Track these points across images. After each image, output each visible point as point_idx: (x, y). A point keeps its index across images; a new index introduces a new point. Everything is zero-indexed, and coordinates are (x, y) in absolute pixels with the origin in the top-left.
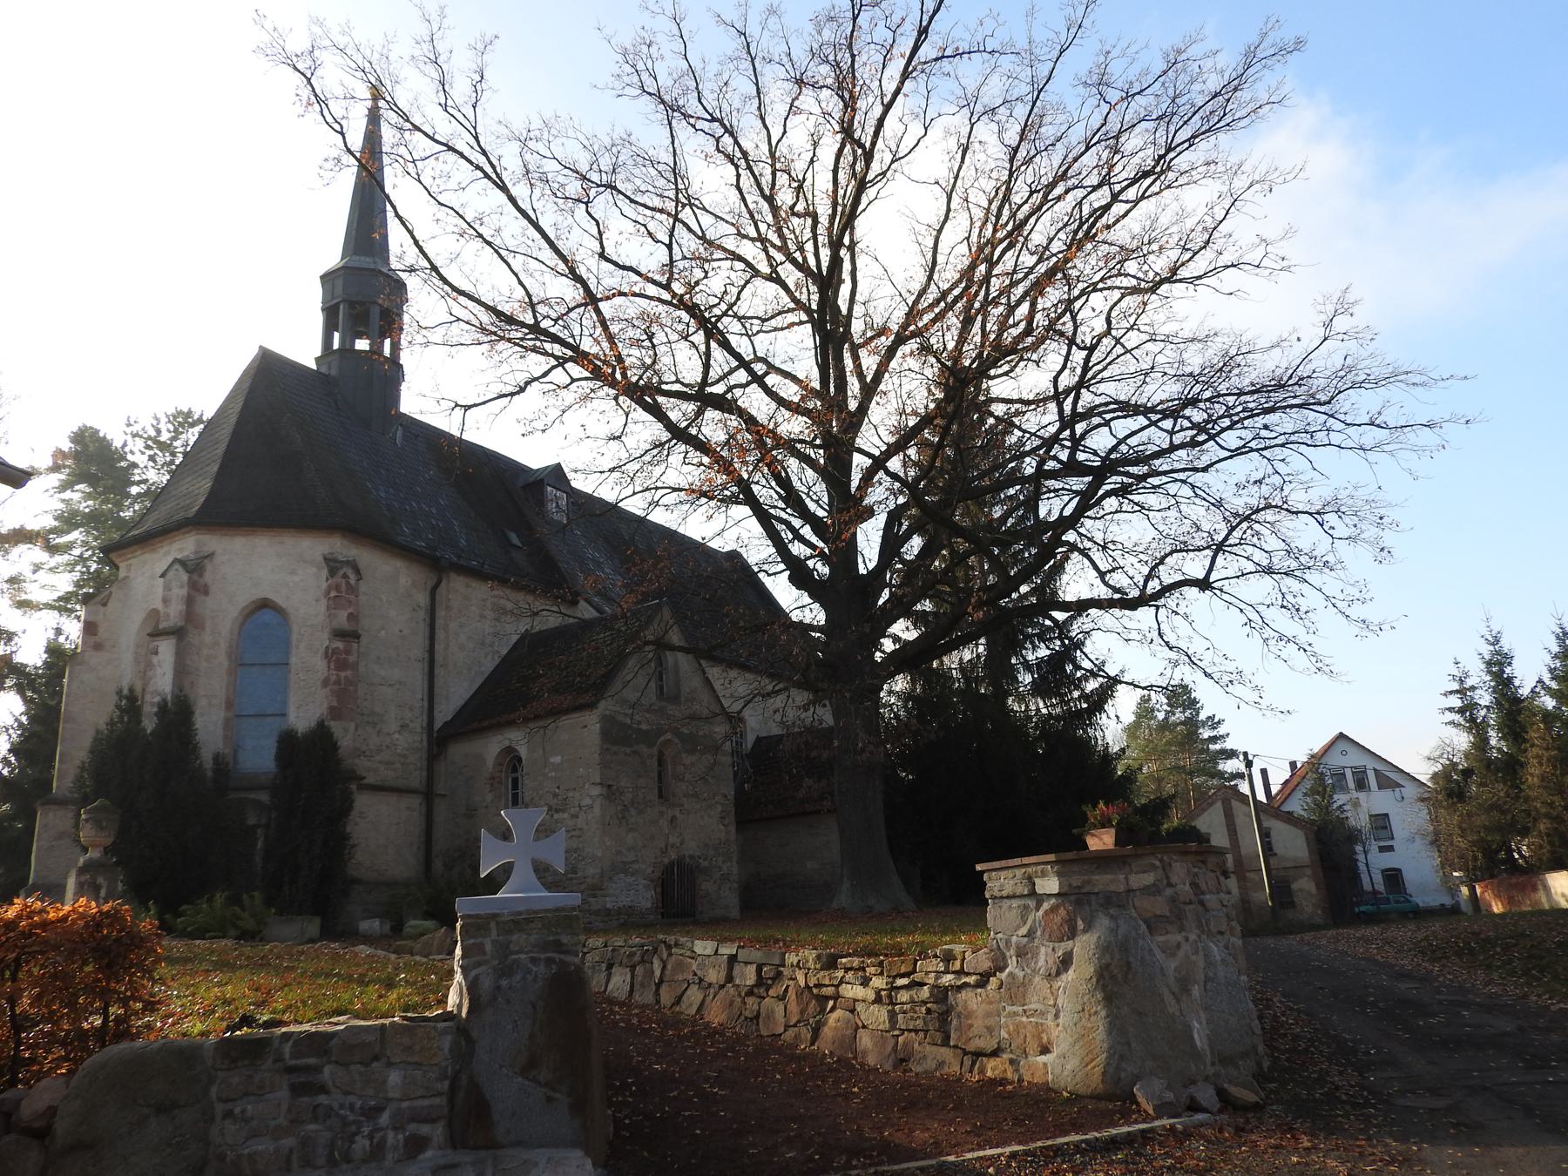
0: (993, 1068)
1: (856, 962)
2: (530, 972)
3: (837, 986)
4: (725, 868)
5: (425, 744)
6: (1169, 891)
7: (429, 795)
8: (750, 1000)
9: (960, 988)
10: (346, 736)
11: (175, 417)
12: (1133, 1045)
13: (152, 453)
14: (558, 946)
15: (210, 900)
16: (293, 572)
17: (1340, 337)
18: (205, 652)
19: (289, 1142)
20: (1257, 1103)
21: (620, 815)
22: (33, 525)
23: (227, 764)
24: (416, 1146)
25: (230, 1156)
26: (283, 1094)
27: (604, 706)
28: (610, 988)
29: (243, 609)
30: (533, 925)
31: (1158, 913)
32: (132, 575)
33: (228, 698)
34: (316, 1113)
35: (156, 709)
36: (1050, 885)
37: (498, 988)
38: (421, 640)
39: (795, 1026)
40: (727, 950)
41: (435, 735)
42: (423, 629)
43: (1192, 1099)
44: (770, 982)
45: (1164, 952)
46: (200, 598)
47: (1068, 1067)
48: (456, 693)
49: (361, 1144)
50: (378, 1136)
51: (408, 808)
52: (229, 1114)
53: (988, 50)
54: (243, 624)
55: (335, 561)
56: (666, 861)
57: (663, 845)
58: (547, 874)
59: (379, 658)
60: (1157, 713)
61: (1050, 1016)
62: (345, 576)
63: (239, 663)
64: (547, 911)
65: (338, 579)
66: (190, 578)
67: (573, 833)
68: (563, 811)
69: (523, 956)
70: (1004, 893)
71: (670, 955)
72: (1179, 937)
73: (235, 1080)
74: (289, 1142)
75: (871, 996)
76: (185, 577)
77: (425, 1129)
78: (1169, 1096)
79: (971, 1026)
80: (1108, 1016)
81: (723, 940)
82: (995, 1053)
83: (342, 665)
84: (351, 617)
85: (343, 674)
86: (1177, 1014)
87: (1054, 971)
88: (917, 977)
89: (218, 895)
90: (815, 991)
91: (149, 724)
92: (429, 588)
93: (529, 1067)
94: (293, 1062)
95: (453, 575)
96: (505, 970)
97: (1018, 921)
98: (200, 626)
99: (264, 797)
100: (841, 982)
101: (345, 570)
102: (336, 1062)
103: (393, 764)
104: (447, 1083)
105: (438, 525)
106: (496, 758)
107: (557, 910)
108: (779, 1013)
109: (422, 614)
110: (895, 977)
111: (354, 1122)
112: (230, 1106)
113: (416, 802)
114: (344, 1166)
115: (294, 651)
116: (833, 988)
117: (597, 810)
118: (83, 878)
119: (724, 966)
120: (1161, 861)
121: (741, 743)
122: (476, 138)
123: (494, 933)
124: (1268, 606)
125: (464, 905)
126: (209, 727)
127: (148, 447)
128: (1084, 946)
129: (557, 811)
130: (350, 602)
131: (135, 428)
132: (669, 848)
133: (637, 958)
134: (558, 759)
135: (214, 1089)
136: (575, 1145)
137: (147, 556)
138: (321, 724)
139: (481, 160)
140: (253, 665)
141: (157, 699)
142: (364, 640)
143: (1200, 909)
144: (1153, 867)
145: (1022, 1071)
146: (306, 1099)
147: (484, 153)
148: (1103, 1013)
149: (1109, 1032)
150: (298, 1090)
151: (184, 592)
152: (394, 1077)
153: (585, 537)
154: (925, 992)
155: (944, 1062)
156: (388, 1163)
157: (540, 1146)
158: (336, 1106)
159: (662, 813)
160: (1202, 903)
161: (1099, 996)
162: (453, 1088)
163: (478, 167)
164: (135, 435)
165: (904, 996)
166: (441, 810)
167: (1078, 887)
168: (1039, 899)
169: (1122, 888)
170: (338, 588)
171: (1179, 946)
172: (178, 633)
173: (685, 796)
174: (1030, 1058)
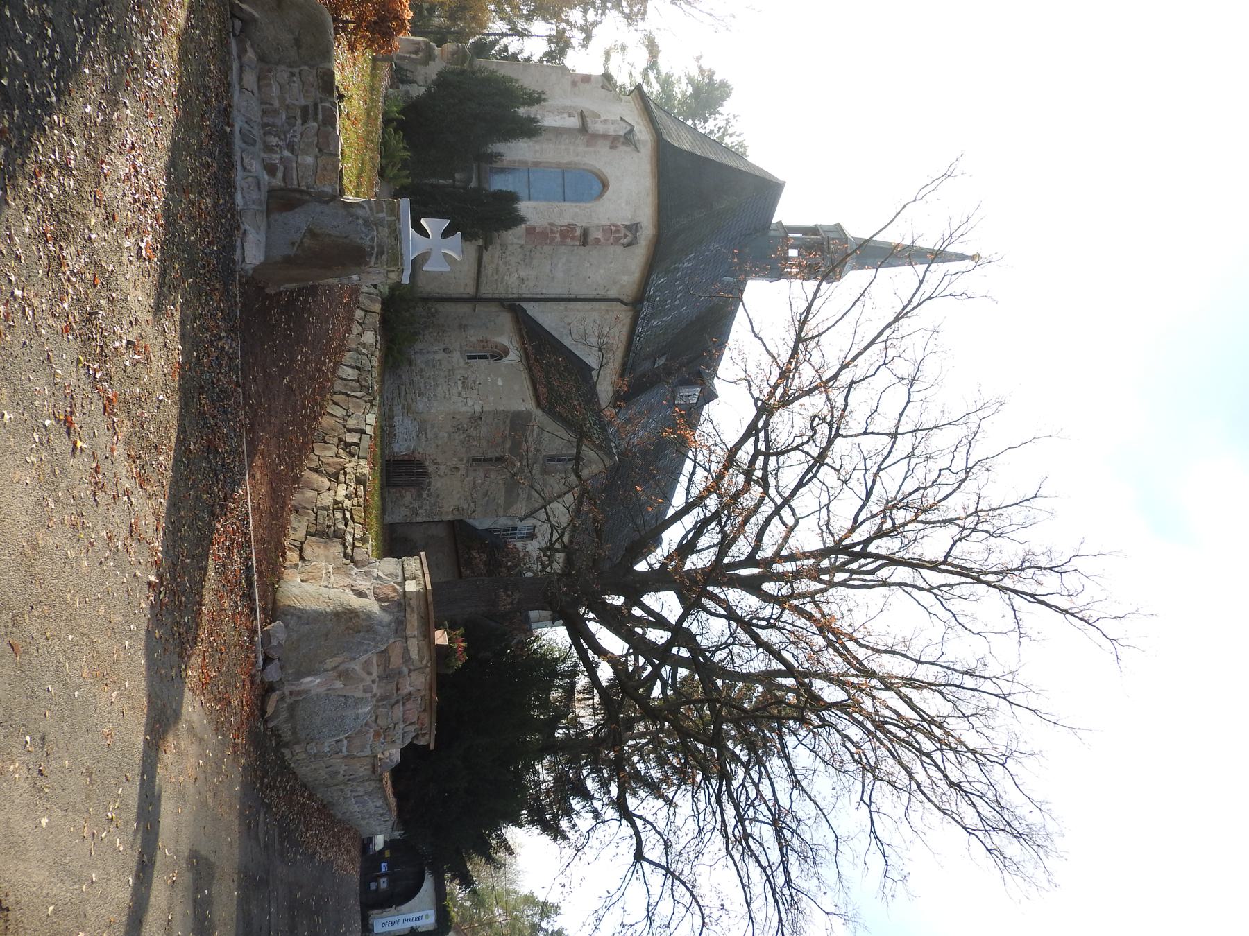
0: (293, 556)
1: (361, 493)
2: (367, 236)
3: (345, 483)
4: (421, 511)
5: (510, 296)
6: (405, 670)
7: (475, 299)
8: (336, 441)
9: (344, 545)
10: (514, 236)
11: (741, 146)
12: (307, 626)
13: (716, 131)
14: (381, 253)
15: (405, 148)
16: (627, 203)
17: (829, 926)
18: (572, 148)
19: (276, 104)
20: (266, 712)
21: (460, 427)
22: (661, 60)
23: (496, 162)
24: (271, 170)
25: (270, 75)
26: (303, 102)
27: (539, 416)
28: (345, 367)
29: (601, 171)
30: (393, 239)
31: (392, 660)
32: (622, 104)
33: (540, 163)
34: (291, 119)
35: (532, 116)
36: (411, 587)
37: (357, 218)
38: (584, 292)
39: (319, 460)
40: (369, 430)
41: (517, 303)
42: (591, 293)
43: (272, 660)
44: (348, 450)
45: (366, 662)
46: (608, 143)
47: (294, 589)
48: (547, 317)
49: (273, 140)
50: (278, 149)
51: (466, 285)
52: (293, 75)
53: (1021, 639)
54: (591, 172)
55: (637, 231)
56: (427, 463)
57: (438, 461)
58: (419, 377)
59: (570, 262)
60: (545, 920)
61: (326, 584)
62: (626, 236)
63: (564, 170)
64: (401, 249)
65: (623, 231)
66: (621, 136)
67: (447, 393)
68: (463, 387)
69: (375, 233)
70: (405, 566)
71: (366, 402)
72: (375, 675)
73: (311, 79)
74: (276, 104)
75: (338, 499)
76: (622, 133)
77: (280, 175)
78: (274, 643)
79: (319, 548)
80: (326, 612)
81: (375, 428)
82: (302, 558)
83: (564, 235)
84: (598, 240)
85: (558, 235)
86: (325, 667)
87: (353, 588)
88: (351, 523)
89: (409, 154)
90: (342, 472)
91: (522, 111)
92: (620, 297)
93: (312, 233)
94: (320, 107)
95: (630, 314)
96: (367, 223)
97: (388, 572)
98: (588, 144)
99: (473, 184)
100: (348, 485)
101: (630, 235)
102: (319, 129)
103: (497, 274)
104: (305, 188)
105: (666, 305)
106: (500, 343)
107: (401, 255)
108: (327, 453)
109: (602, 292)
110: (351, 512)
111: (286, 137)
112: (297, 75)
113: (471, 290)
114: (262, 132)
115: (573, 204)
116: (344, 480)
117: (464, 409)
118: (422, 44)
119: (359, 427)
120: (426, 666)
121: (515, 538)
122: (929, 298)
123: (389, 219)
124: (623, 908)
125: (405, 203)
126: (518, 151)
127: (720, 128)
128: (370, 605)
129: (463, 383)
130: (608, 240)
131: (732, 121)
132: (436, 466)
133: (364, 383)
134: (500, 383)
135: (306, 68)
136: (267, 257)
137: (636, 112)
138: (522, 220)
139: (914, 303)
140: (563, 179)
141: (539, 117)
142: (582, 250)
143: (393, 701)
144: (421, 659)
145: (291, 570)
146: (299, 113)
147: (919, 305)
148: (328, 610)
149: (316, 611)
150: (305, 110)
151: (612, 132)
152: (309, 160)
153: (665, 418)
154: (341, 526)
155: (296, 531)
156: (263, 155)
157: (267, 238)
158: (295, 128)
159: (461, 460)
160: (397, 702)
161: (339, 609)
162: (301, 191)
163: (910, 301)
164: (727, 121)
165: (339, 515)
166: (465, 308)
167: (409, 604)
168: (402, 584)
169: (408, 632)
170: (617, 231)
171: (369, 674)
172: (584, 129)
173: (474, 478)
174: (299, 575)
